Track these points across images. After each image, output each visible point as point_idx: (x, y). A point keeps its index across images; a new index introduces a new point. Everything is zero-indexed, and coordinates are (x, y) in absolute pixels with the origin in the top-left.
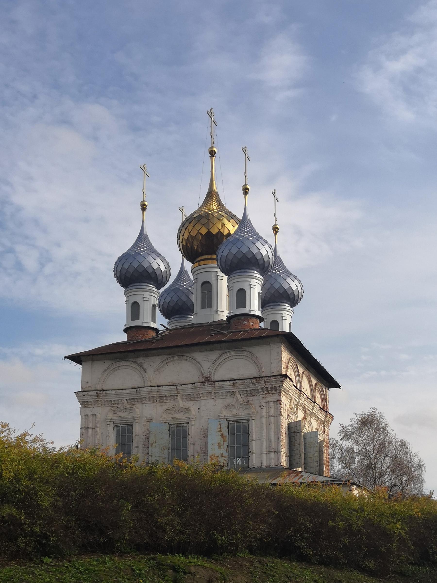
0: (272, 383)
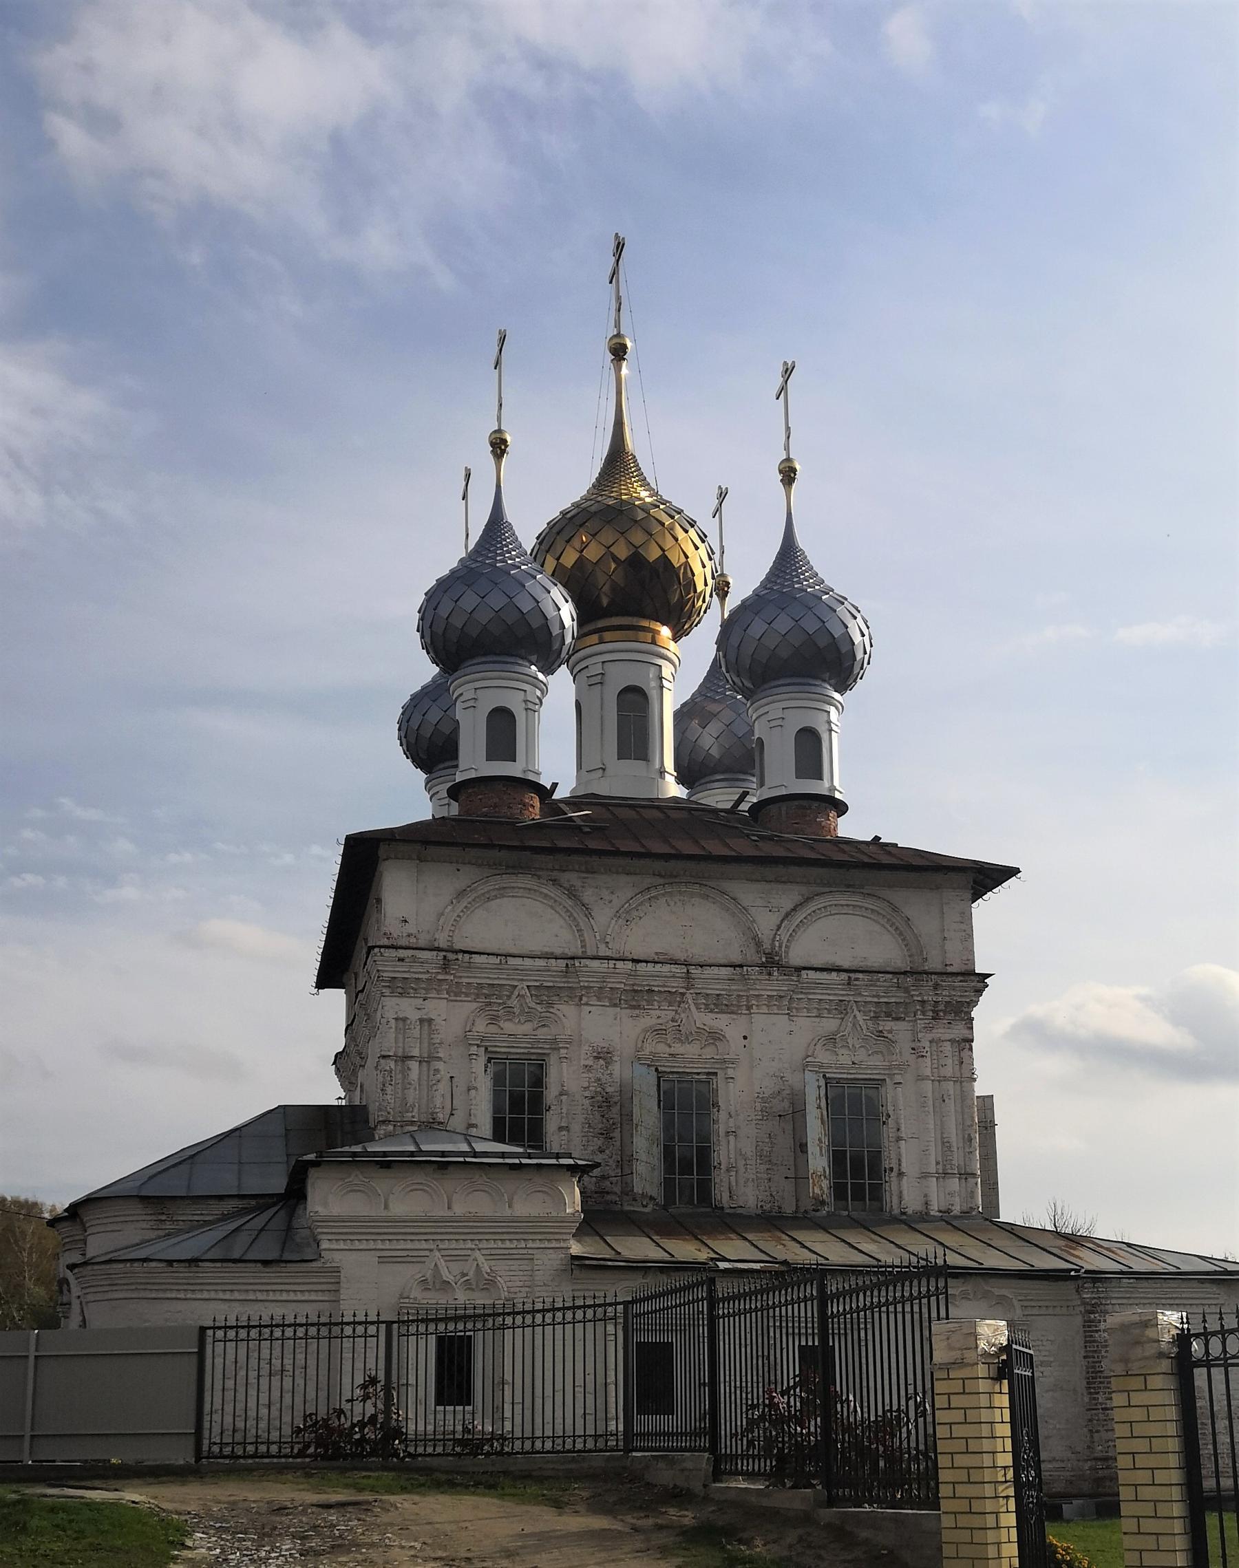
0: (951, 991)
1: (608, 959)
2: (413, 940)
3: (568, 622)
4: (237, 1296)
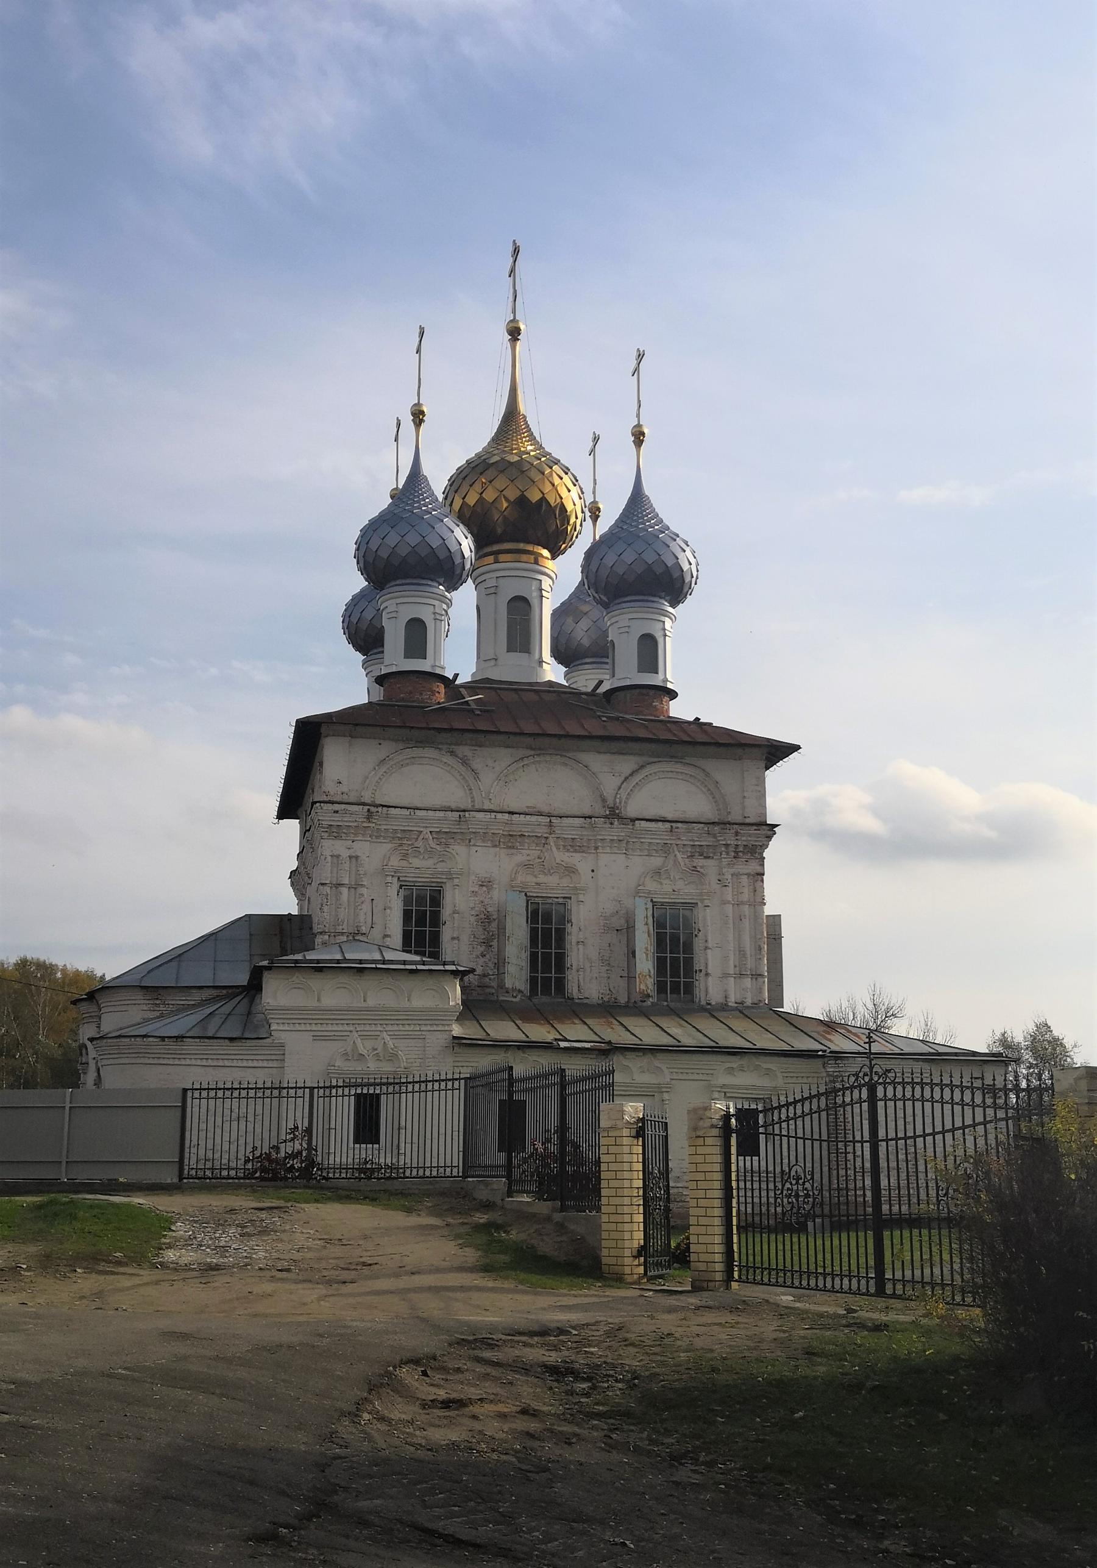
0: (748, 836)
4: (210, 1063)
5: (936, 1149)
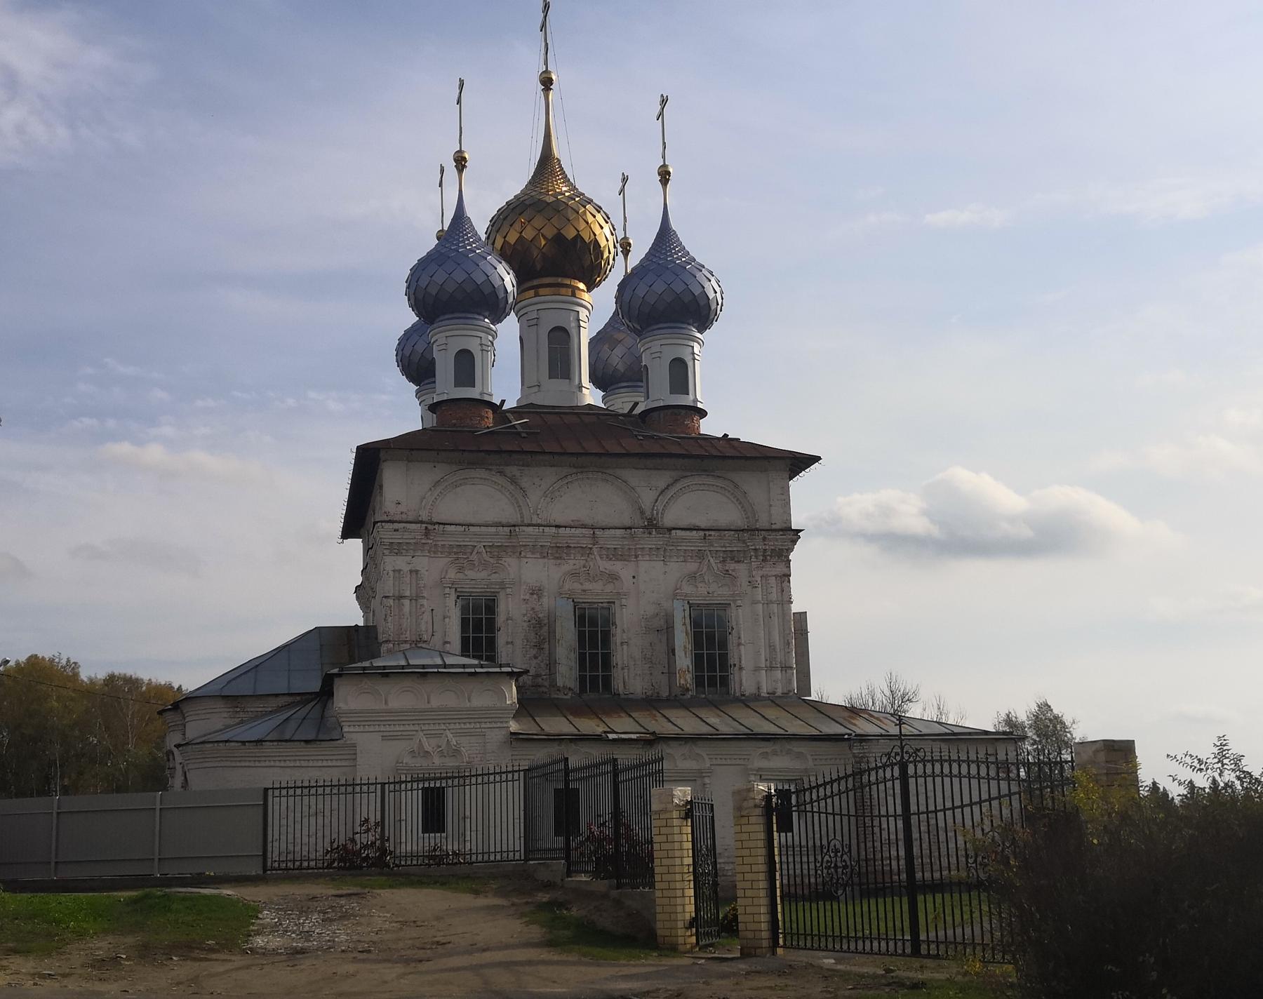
0: (776, 541)
1: (539, 525)
2: (404, 516)
3: (509, 288)
4: (288, 764)
5: (964, 818)
